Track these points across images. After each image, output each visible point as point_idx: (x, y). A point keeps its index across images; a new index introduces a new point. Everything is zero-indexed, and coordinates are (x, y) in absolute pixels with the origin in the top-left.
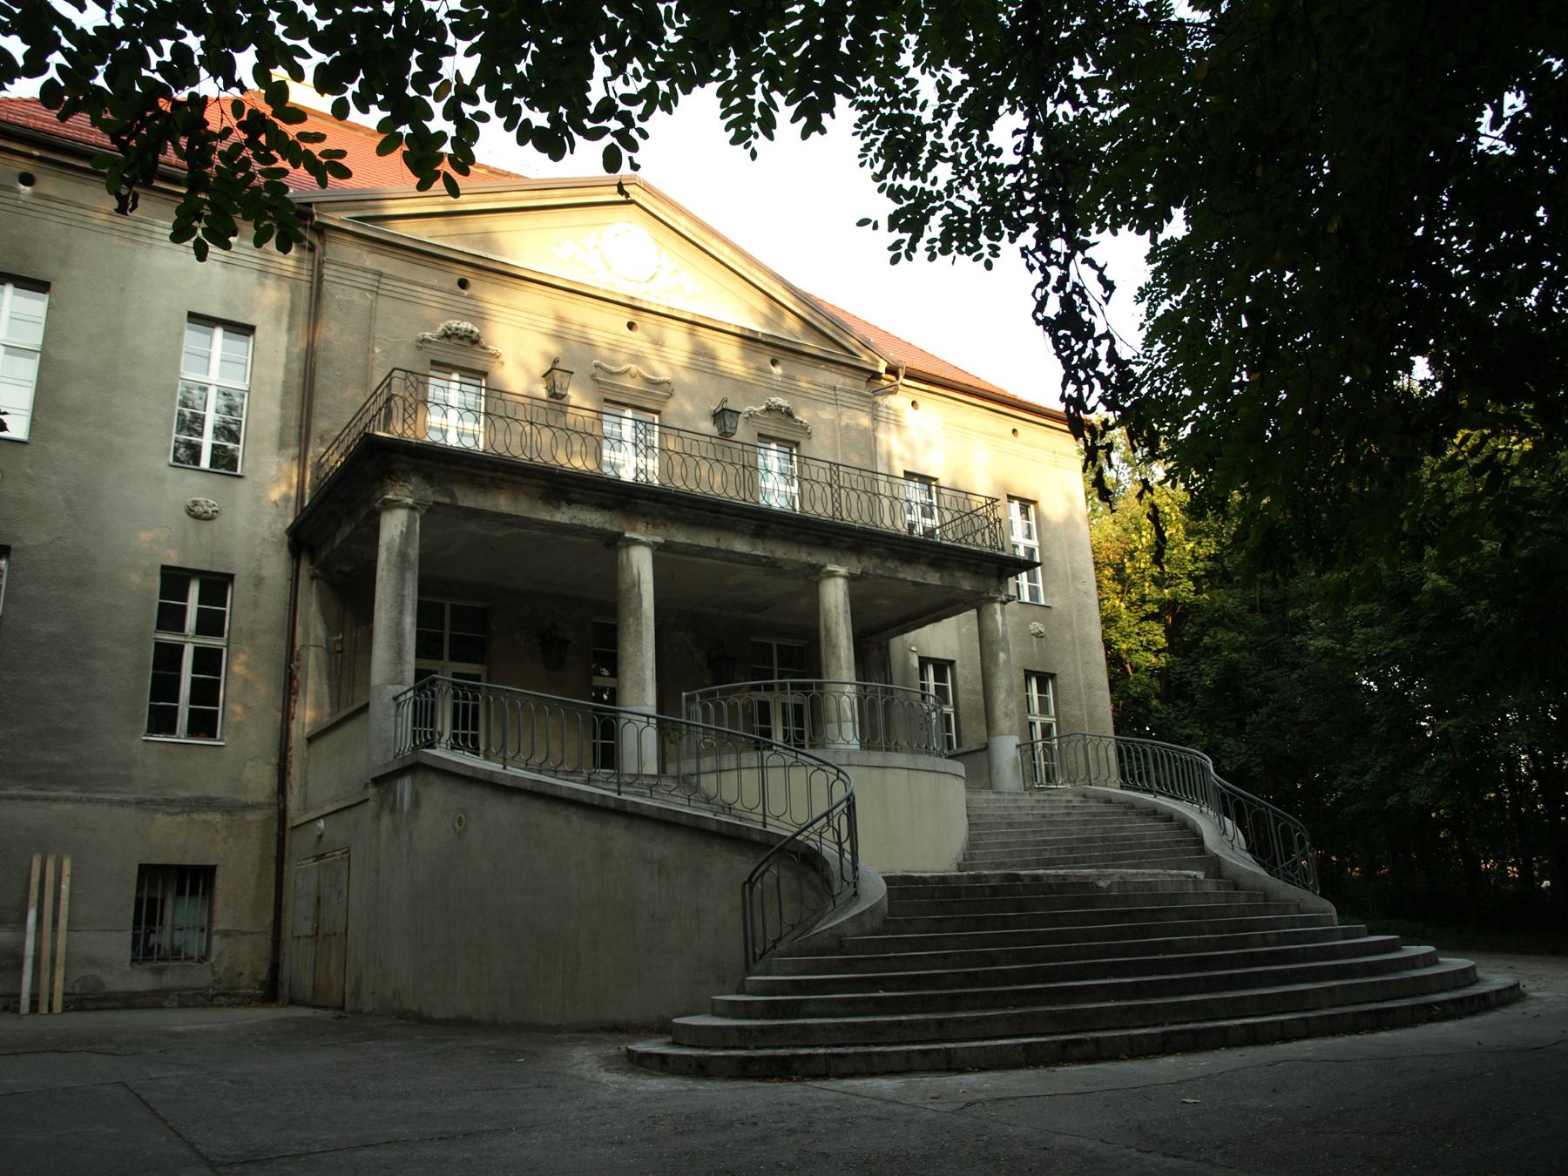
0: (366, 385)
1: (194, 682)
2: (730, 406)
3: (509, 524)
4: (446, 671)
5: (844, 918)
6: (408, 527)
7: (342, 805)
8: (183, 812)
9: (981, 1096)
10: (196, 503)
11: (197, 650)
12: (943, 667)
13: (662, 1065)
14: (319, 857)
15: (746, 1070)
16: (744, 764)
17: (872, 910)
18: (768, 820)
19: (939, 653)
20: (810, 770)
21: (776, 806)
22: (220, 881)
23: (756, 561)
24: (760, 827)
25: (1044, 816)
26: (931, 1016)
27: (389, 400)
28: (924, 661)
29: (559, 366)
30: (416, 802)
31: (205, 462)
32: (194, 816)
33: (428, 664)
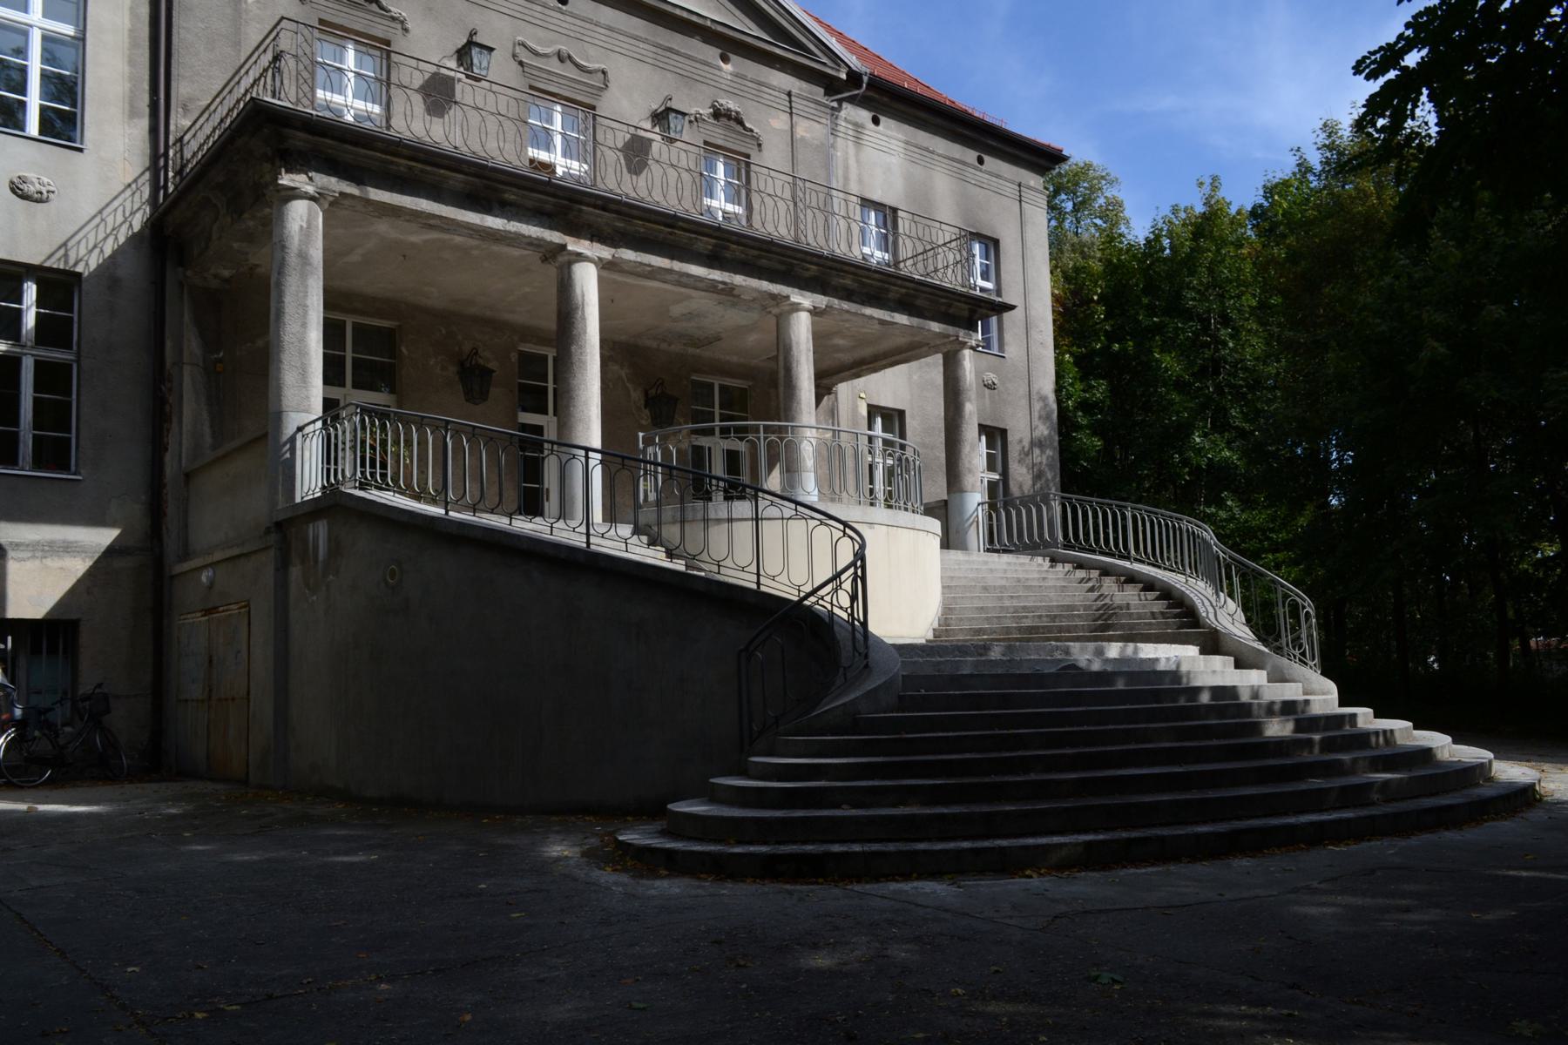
0: (237, 44)
1: (37, 402)
2: (674, 105)
3: (431, 227)
4: (352, 396)
5: (858, 693)
6: (309, 223)
7: (236, 551)
8: (34, 557)
9: (1063, 908)
10: (23, 180)
11: (39, 365)
12: (893, 418)
13: (672, 864)
14: (208, 612)
15: (770, 869)
16: (689, 515)
17: (887, 685)
18: (762, 580)
19: (887, 401)
20: (812, 523)
21: (771, 564)
22: (85, 637)
23: (712, 287)
24: (754, 586)
25: (1019, 580)
26: (976, 809)
27: (277, 58)
28: (873, 410)
29: (477, 39)
30: (335, 549)
31: (33, 127)
32: (48, 562)
33: (336, 393)
